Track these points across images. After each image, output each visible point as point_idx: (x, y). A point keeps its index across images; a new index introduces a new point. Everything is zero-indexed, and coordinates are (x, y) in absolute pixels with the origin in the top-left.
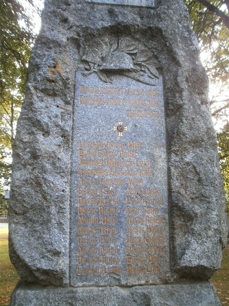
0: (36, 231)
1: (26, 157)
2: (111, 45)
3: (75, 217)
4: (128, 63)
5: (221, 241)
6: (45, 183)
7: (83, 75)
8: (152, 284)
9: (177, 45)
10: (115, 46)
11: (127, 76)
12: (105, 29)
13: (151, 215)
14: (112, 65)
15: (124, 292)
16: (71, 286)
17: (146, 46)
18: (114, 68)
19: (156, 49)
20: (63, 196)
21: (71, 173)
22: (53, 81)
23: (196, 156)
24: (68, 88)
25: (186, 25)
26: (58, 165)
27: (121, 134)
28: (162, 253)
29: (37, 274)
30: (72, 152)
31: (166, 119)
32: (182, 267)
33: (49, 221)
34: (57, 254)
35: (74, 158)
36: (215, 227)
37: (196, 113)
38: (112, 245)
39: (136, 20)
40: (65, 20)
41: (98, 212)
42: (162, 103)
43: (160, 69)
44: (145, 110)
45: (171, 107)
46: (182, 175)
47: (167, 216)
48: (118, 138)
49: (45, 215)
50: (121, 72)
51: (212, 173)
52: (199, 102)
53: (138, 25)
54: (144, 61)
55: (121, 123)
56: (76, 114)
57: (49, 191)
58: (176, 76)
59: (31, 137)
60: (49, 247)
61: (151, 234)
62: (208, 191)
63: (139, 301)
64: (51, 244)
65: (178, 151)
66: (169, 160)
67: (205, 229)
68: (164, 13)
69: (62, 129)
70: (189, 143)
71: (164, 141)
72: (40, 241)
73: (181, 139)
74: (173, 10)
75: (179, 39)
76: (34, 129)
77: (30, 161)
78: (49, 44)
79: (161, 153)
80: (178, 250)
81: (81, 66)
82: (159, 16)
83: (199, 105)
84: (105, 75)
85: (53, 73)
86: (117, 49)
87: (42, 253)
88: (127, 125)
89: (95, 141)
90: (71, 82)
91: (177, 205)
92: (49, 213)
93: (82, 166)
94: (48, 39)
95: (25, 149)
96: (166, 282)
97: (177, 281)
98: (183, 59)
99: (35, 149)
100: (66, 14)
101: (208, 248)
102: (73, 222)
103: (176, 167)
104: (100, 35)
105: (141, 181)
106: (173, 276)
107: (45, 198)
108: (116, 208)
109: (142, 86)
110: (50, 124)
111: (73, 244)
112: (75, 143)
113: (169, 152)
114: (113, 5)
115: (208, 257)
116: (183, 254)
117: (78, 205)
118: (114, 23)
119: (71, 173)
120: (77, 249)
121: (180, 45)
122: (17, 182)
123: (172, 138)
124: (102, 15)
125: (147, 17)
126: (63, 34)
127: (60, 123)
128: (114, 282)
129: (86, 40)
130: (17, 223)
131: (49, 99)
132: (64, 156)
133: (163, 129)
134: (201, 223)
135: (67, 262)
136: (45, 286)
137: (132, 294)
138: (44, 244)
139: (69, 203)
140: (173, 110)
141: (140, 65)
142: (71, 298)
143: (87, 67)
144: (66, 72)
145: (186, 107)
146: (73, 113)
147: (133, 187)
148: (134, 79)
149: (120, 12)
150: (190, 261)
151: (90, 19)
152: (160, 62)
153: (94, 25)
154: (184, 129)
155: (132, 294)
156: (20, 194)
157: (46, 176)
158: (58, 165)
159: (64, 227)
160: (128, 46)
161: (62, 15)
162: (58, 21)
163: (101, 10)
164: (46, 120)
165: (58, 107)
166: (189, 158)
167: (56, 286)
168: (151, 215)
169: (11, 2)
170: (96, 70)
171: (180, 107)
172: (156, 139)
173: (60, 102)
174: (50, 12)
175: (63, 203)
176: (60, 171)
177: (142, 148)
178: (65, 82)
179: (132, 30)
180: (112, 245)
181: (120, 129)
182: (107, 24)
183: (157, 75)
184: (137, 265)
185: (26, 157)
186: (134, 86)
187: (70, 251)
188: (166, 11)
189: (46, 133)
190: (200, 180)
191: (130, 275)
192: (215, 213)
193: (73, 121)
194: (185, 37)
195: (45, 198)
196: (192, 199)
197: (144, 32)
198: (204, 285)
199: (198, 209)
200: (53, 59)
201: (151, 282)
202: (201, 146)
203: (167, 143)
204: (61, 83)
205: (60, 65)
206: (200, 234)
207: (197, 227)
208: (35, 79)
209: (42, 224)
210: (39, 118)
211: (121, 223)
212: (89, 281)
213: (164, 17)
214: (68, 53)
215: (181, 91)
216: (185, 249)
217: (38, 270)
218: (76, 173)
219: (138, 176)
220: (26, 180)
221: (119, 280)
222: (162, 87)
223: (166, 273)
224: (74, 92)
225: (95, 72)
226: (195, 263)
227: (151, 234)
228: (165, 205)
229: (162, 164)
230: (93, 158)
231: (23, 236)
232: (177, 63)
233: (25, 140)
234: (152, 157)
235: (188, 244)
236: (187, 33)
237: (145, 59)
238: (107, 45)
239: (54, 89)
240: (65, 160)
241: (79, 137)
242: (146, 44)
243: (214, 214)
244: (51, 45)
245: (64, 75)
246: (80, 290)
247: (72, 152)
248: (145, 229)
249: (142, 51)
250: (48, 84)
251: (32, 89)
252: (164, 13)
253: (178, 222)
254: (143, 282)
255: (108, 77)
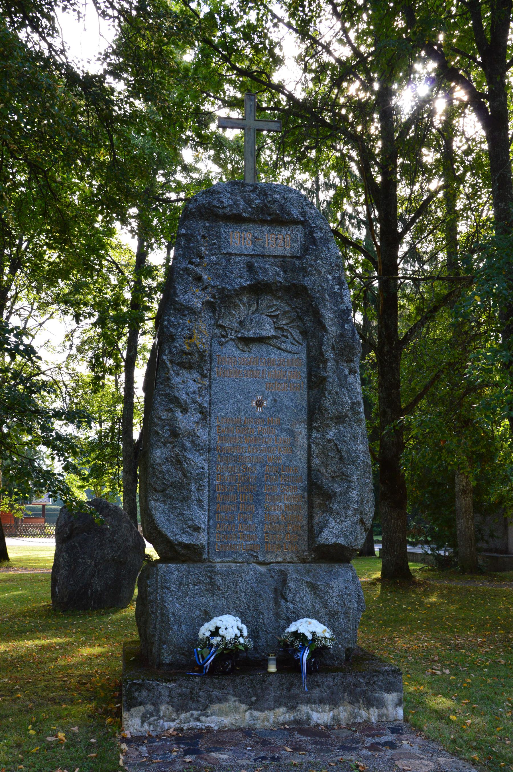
0: (176, 508)
1: (166, 435)
2: (250, 306)
3: (214, 494)
4: (268, 330)
5: (362, 521)
6: (185, 461)
7: (219, 342)
8: (289, 562)
9: (325, 305)
10: (254, 308)
11: (268, 344)
12: (243, 289)
13: (289, 493)
14: (251, 332)
15: (262, 569)
16: (209, 561)
17: (289, 305)
18: (253, 336)
19: (300, 309)
20: (203, 474)
21: (209, 450)
22: (189, 354)
23: (339, 433)
24: (205, 360)
25: (337, 275)
26: (197, 442)
27: (259, 410)
28: (300, 532)
29: (178, 548)
30: (210, 428)
31: (308, 392)
32: (319, 545)
33: (189, 498)
34: (197, 529)
35: (212, 435)
36: (355, 506)
37: (340, 385)
38: (250, 523)
39: (278, 275)
40: (199, 279)
41: (236, 490)
42: (305, 374)
43: (304, 333)
44: (286, 383)
45: (314, 379)
46: (323, 453)
47: (306, 494)
48: (257, 414)
49: (185, 492)
50: (261, 340)
51: (355, 451)
52: (347, 372)
53: (280, 282)
54: (286, 324)
55: (259, 398)
56: (213, 387)
57: (189, 469)
58: (321, 344)
59: (170, 414)
60: (190, 523)
61: (289, 512)
62: (350, 469)
63: (276, 577)
64: (192, 520)
65: (319, 427)
66: (309, 437)
67: (344, 508)
68: (311, 266)
69: (200, 406)
70: (332, 419)
71: (305, 417)
72: (181, 518)
73: (323, 415)
74: (322, 259)
75: (327, 297)
76: (172, 406)
77: (170, 439)
78: (184, 311)
79: (301, 429)
80: (316, 529)
81: (217, 331)
82: (304, 269)
83: (346, 376)
84: (243, 343)
85: (189, 345)
86: (257, 310)
87: (183, 529)
88: (266, 399)
89: (233, 416)
90: (207, 353)
91: (316, 484)
92: (189, 490)
93: (220, 443)
94: (182, 305)
95: (164, 427)
96: (303, 561)
97: (315, 561)
98: (330, 323)
99: (175, 427)
100: (199, 271)
101: (346, 527)
102: (212, 499)
103: (317, 444)
104: (237, 295)
105: (279, 458)
106: (310, 555)
107: (185, 475)
108: (254, 485)
109: (283, 354)
110: (188, 401)
111: (211, 521)
112: (213, 419)
113: (310, 428)
114: (252, 256)
115: (346, 536)
116: (321, 532)
117: (216, 483)
118: (275, 662)
119: (209, 450)
120: (215, 526)
121: (328, 304)
122: (158, 459)
123: (314, 413)
124: (239, 270)
125: (291, 270)
126: (198, 297)
127: (198, 399)
128: (252, 559)
129: (222, 302)
130: (157, 500)
131: (185, 373)
132: (202, 433)
133: (304, 404)
134: (339, 502)
135: (206, 538)
136: (183, 562)
137: (270, 570)
138: (184, 520)
139: (207, 480)
140: (316, 383)
141: (282, 329)
142: (210, 572)
143: (224, 333)
144: (202, 343)
145: (330, 380)
146: (210, 386)
147: (271, 464)
148: (274, 346)
149: (260, 268)
150: (327, 539)
151: (226, 275)
152: (304, 324)
153: (231, 284)
154: (327, 404)
155: (270, 570)
156: (160, 472)
157: (186, 454)
158: (197, 442)
159: (204, 504)
160: (269, 307)
161: (196, 273)
162: (191, 279)
163: (239, 263)
164: (184, 396)
165: (194, 381)
166: (330, 435)
167: (195, 561)
168: (289, 493)
169: (375, 703)
170: (233, 337)
171: (323, 380)
172: (296, 414)
173: (196, 375)
174: (182, 270)
175: (202, 480)
176: (198, 449)
177: (281, 424)
178: (202, 356)
179: (274, 288)
180: (250, 523)
181: (259, 404)
182: (245, 283)
183: (301, 341)
184: (275, 543)
185: (166, 435)
186: (275, 355)
187: (209, 528)
188: (313, 263)
189: (185, 410)
190: (341, 458)
191: (267, 552)
192: (355, 492)
193: (210, 395)
194: (335, 293)
195: (185, 475)
196: (333, 477)
197: (287, 289)
198: (342, 565)
199: (337, 489)
200: (189, 330)
201: (288, 560)
202: (344, 422)
203: (308, 418)
204: (197, 355)
205: (195, 335)
206: (338, 513)
207: (335, 506)
208: (171, 352)
209: (182, 501)
210: (177, 394)
211: (259, 500)
212: (228, 557)
213: (311, 271)
214: (203, 319)
215: (326, 362)
216: (322, 528)
217: (180, 543)
218: (215, 450)
219: (277, 453)
220: (167, 458)
221: (257, 557)
222: (305, 355)
223: (304, 551)
224: (211, 363)
225: (232, 339)
226: (332, 541)
227: (289, 512)
228: (304, 483)
229: (302, 441)
230: (231, 435)
231: (163, 512)
232: (324, 328)
233: (163, 418)
234: (291, 433)
235: (326, 523)
236: (338, 287)
237: (287, 321)
238: (245, 306)
239: (190, 362)
240: (203, 437)
241: (217, 413)
242: (290, 302)
243: (354, 494)
244: (186, 313)
245: (200, 346)
246: (218, 565)
247: (210, 428)
248: (283, 507)
249: (285, 313)
250: (184, 356)
251: (168, 362)
252: (311, 266)
253: (317, 501)
254: (280, 560)
255: (247, 345)
